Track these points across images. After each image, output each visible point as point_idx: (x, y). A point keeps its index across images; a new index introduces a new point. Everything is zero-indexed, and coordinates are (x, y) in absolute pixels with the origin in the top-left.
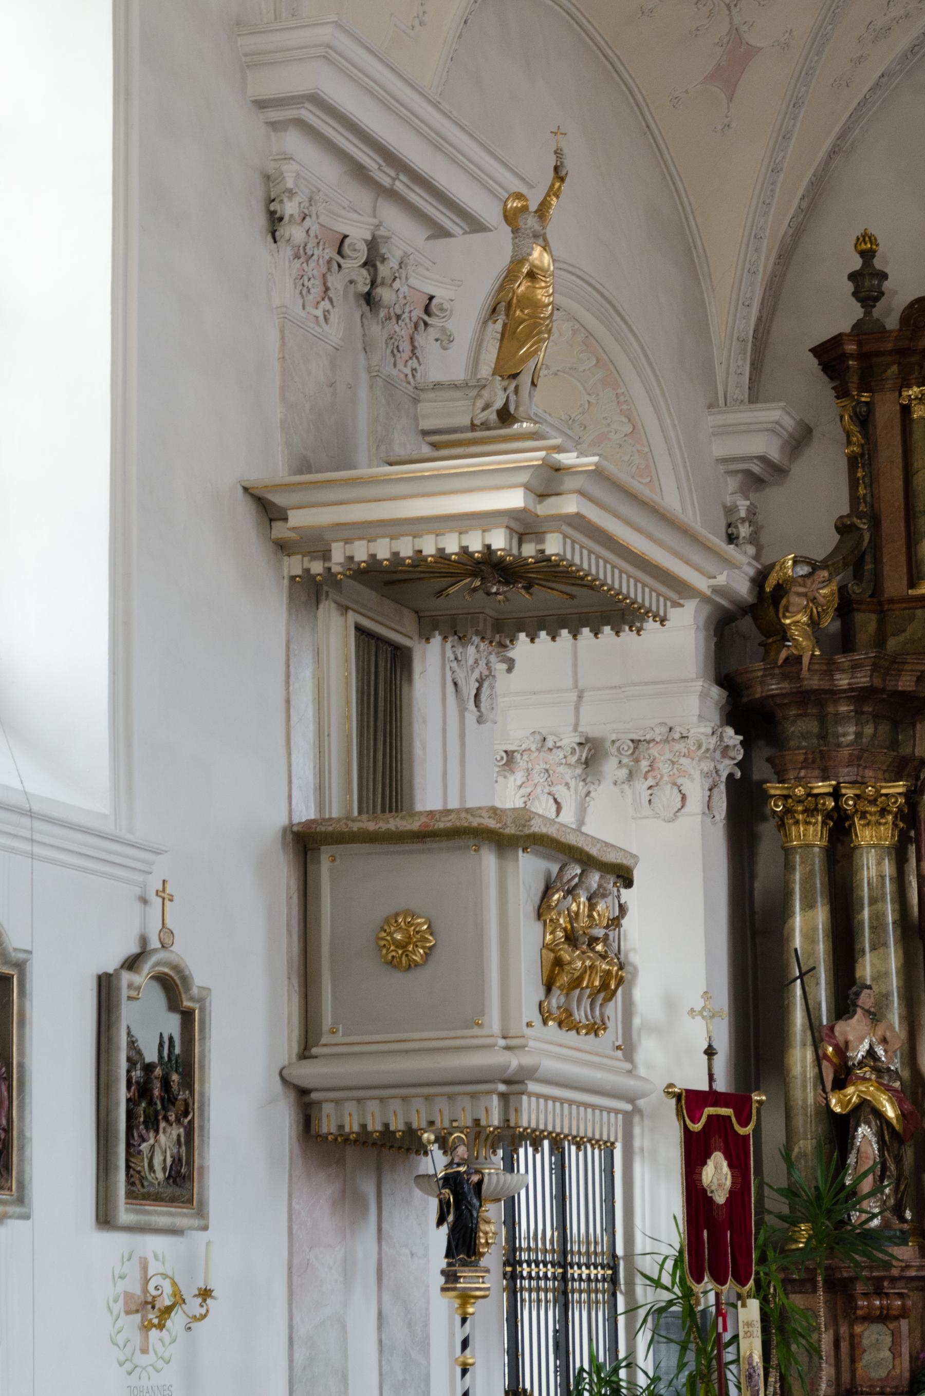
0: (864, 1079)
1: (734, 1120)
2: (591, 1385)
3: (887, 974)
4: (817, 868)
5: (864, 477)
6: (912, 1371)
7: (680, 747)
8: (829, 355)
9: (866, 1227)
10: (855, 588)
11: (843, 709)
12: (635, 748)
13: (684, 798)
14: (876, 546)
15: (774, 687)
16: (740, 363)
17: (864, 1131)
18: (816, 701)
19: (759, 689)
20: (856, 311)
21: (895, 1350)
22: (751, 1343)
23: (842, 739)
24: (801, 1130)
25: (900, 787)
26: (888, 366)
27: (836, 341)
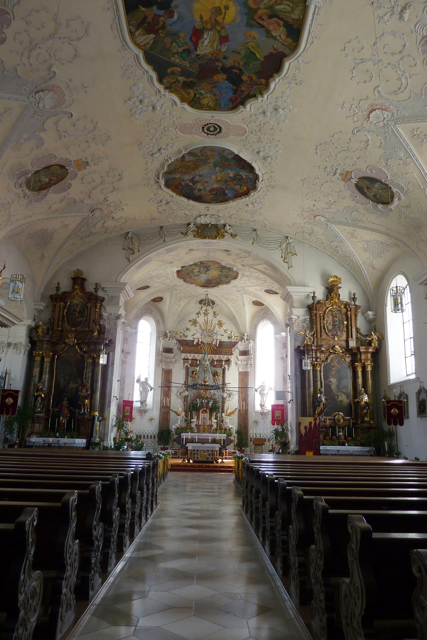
7: (21, 345)
14: (53, 323)
15: (36, 339)
17: (39, 398)
21: (40, 428)
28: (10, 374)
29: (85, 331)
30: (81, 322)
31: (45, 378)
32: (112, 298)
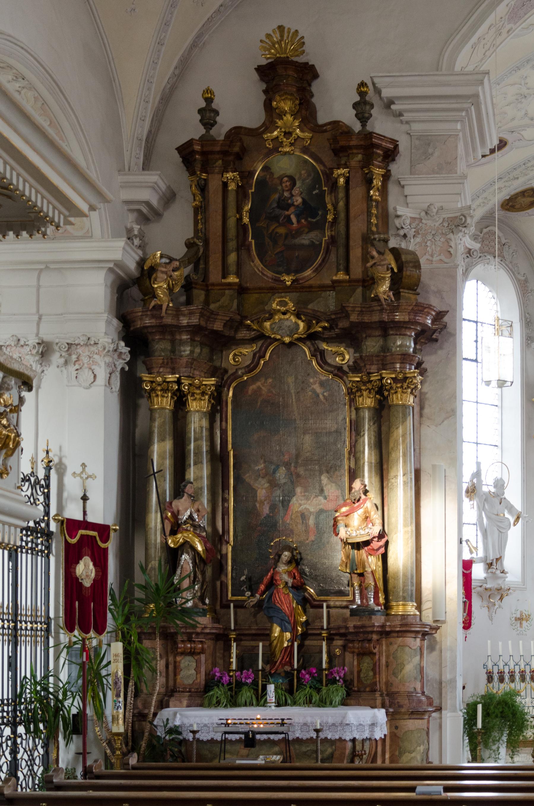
0: (187, 530)
1: (98, 538)
2: (31, 686)
3: (202, 478)
4: (167, 420)
5: (201, 219)
6: (206, 680)
7: (94, 349)
8: (186, 152)
9: (184, 606)
10: (194, 276)
11: (184, 337)
12: (69, 348)
13: (95, 376)
14: (206, 256)
15: (148, 322)
16: (138, 152)
17: (185, 557)
18: (169, 331)
19: (139, 323)
20: (202, 131)
21: (197, 670)
22: (117, 666)
23: (183, 353)
24: (153, 556)
25: (212, 381)
26: (217, 160)
27: (190, 143)
28: (61, 470)
29: (335, 285)
30: (315, 247)
31: (199, 478)
32: (426, 143)
